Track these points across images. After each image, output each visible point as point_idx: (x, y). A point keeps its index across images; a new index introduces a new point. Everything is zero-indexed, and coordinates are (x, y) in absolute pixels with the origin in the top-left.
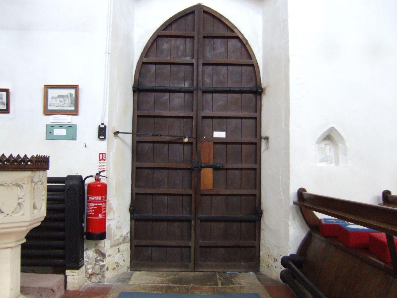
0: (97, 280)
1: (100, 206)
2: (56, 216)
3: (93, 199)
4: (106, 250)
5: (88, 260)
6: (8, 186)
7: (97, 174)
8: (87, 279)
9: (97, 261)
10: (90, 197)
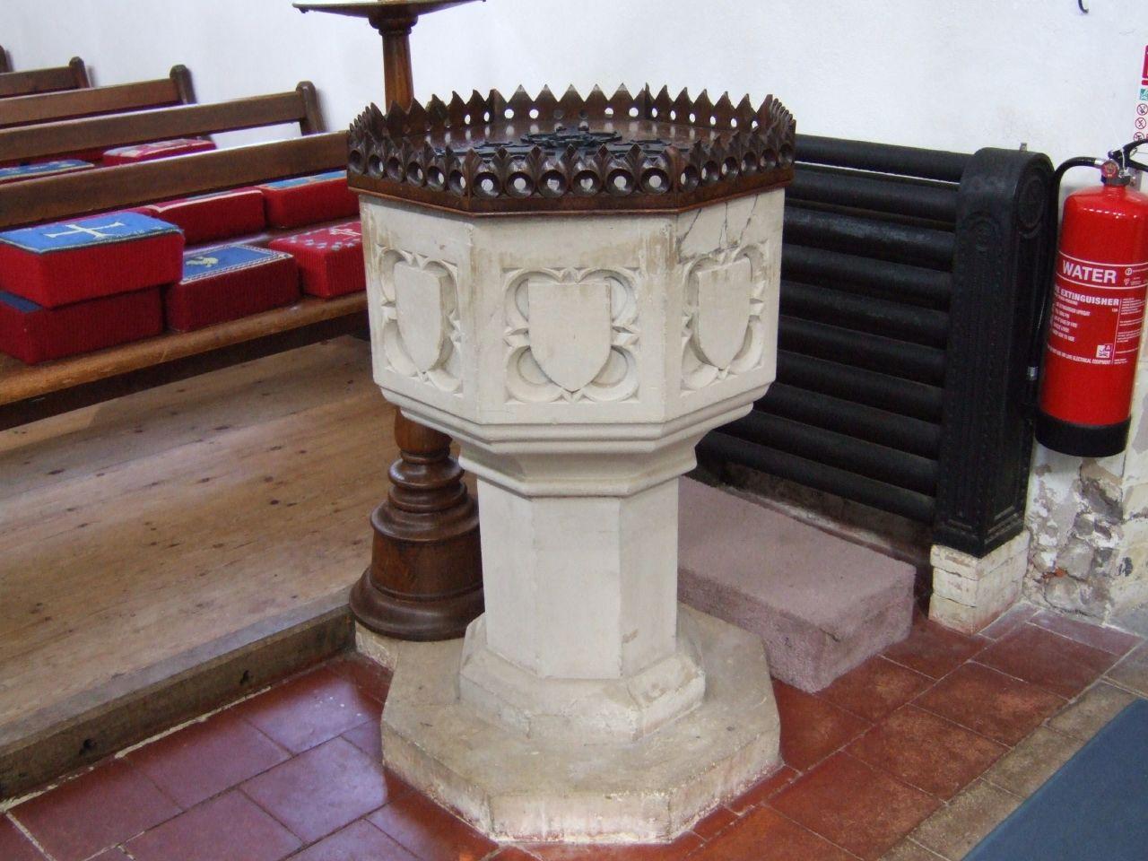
0: (1073, 601)
1: (1108, 308)
3: (1077, 271)
4: (1131, 490)
5: (1044, 513)
6: (567, 277)
7: (1116, 156)
8: (1031, 583)
9: (1080, 524)
10: (1067, 260)
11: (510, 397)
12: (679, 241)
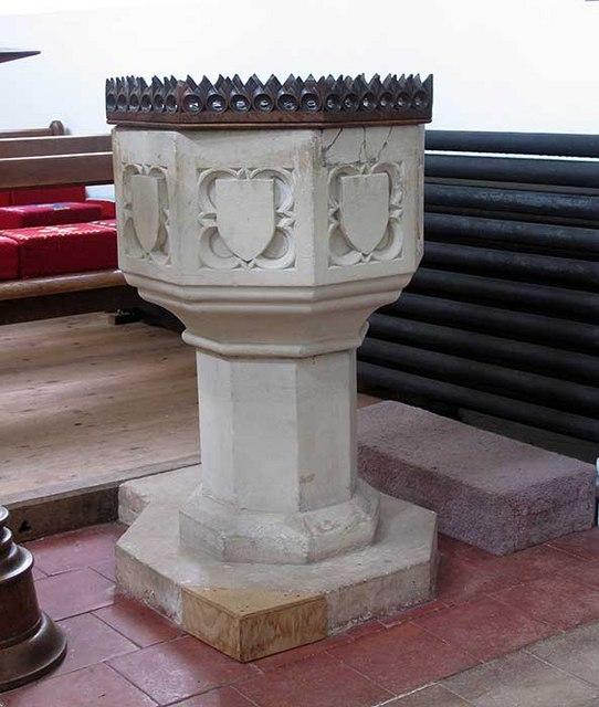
2: (442, 277)
6: (243, 176)
11: (203, 265)
12: (324, 151)
